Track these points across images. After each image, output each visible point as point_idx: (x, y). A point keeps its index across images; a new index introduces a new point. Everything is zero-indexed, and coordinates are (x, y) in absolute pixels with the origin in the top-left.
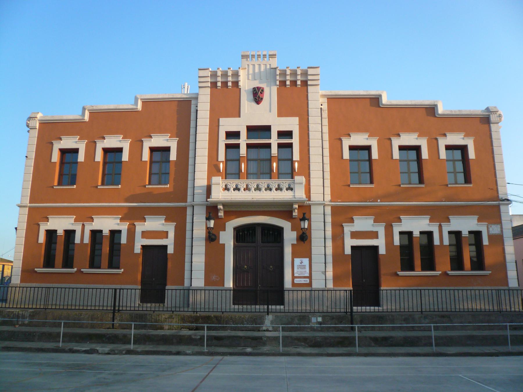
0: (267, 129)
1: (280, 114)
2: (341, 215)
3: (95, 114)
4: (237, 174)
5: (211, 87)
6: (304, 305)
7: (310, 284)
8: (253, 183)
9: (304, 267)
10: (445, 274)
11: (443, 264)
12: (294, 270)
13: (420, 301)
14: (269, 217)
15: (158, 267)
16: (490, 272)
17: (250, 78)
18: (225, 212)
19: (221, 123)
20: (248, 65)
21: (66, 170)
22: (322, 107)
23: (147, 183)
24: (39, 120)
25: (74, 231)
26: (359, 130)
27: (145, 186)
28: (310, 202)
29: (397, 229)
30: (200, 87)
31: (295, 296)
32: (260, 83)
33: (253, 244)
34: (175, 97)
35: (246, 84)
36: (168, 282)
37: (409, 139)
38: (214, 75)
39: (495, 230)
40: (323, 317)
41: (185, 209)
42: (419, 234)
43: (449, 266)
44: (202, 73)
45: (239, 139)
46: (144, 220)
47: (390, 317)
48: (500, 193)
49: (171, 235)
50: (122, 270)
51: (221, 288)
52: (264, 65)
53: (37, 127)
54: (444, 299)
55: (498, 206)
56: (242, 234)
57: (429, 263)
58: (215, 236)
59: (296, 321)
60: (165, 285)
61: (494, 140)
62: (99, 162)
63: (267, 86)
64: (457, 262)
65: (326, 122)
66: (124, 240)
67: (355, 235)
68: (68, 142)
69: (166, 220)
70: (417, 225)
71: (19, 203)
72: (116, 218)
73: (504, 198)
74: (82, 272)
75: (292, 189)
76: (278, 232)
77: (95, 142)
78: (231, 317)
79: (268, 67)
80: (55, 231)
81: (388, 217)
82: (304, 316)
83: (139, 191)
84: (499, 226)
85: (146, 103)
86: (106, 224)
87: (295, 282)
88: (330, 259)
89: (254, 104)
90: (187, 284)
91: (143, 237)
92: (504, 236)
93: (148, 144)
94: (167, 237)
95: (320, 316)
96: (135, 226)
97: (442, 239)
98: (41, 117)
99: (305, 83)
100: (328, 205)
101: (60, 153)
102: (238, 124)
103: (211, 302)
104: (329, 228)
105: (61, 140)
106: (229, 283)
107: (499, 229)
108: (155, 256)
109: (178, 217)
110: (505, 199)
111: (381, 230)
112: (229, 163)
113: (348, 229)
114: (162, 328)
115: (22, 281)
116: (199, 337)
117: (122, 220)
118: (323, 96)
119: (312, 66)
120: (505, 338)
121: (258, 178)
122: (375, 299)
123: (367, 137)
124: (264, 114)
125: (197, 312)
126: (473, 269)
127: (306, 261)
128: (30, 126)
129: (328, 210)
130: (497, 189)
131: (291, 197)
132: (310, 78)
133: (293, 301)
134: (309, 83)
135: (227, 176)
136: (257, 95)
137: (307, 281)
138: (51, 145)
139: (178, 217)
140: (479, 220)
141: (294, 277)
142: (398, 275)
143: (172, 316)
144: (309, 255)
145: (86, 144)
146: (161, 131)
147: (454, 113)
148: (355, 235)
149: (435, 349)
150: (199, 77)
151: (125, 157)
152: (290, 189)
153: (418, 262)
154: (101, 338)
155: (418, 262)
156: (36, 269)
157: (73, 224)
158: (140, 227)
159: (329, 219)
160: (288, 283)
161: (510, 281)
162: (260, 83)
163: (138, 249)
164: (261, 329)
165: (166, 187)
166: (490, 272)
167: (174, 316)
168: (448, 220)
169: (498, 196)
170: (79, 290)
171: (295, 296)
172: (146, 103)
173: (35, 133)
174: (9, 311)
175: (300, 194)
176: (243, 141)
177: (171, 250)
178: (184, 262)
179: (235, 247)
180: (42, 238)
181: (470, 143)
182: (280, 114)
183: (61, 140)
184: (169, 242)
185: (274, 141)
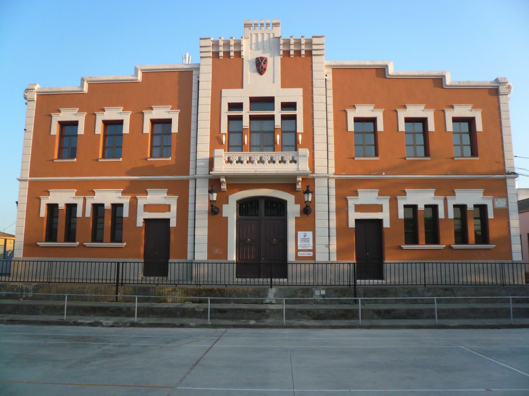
0: (270, 100)
2: (346, 188)
6: (307, 278)
7: (314, 257)
8: (256, 155)
10: (449, 247)
11: (447, 237)
12: (298, 243)
16: (495, 246)
20: (251, 34)
22: (327, 77)
23: (149, 156)
24: (37, 92)
26: (365, 101)
27: (146, 159)
28: (314, 175)
29: (401, 202)
30: (201, 57)
32: (263, 53)
35: (249, 54)
37: (415, 111)
38: (216, 44)
39: (501, 203)
40: (327, 290)
41: (187, 181)
44: (204, 43)
46: (146, 193)
47: (394, 289)
48: (506, 166)
49: (174, 208)
50: (125, 244)
53: (35, 99)
54: (448, 273)
55: (504, 180)
56: (245, 207)
57: (433, 237)
58: (218, 209)
60: (168, 258)
62: (55, 135)
63: (271, 56)
64: (462, 236)
65: (330, 93)
66: (126, 213)
67: (359, 208)
69: (169, 193)
72: (118, 192)
74: (85, 245)
75: (295, 162)
76: (282, 204)
77: (95, 115)
78: (235, 290)
79: (272, 36)
80: (57, 205)
81: (393, 190)
84: (505, 200)
86: (108, 197)
87: (299, 255)
88: (334, 232)
89: (257, 75)
90: (190, 257)
92: (510, 210)
95: (323, 289)
97: (447, 212)
99: (309, 53)
100: (333, 178)
102: (241, 96)
103: (214, 275)
104: (333, 201)
105: (153, 110)
106: (232, 256)
107: (505, 203)
108: (157, 229)
109: (180, 190)
111: (385, 203)
113: (352, 202)
114: (165, 301)
116: (202, 310)
117: (123, 193)
118: (328, 66)
121: (262, 150)
124: (268, 85)
126: (477, 243)
127: (309, 234)
128: (28, 97)
129: (332, 183)
130: (504, 162)
131: (295, 170)
132: (314, 47)
133: (297, 275)
134: (314, 53)
136: (260, 66)
137: (311, 254)
138: (50, 118)
139: (180, 190)
140: (485, 194)
141: (297, 250)
144: (312, 228)
146: (162, 102)
147: (462, 84)
148: (359, 208)
149: (437, 321)
150: (201, 47)
151: (126, 129)
152: (294, 161)
153: (422, 235)
154: (104, 311)
155: (422, 235)
156: (38, 243)
158: (142, 201)
159: (333, 192)
160: (291, 257)
161: (514, 255)
162: (263, 53)
163: (140, 223)
166: (495, 246)
167: (177, 289)
168: (454, 194)
169: (505, 170)
170: (78, 264)
175: (303, 166)
176: (246, 113)
177: (173, 224)
180: (43, 212)
181: (478, 115)
182: (284, 86)
183: (153, 110)
184: (172, 215)
185: (278, 112)
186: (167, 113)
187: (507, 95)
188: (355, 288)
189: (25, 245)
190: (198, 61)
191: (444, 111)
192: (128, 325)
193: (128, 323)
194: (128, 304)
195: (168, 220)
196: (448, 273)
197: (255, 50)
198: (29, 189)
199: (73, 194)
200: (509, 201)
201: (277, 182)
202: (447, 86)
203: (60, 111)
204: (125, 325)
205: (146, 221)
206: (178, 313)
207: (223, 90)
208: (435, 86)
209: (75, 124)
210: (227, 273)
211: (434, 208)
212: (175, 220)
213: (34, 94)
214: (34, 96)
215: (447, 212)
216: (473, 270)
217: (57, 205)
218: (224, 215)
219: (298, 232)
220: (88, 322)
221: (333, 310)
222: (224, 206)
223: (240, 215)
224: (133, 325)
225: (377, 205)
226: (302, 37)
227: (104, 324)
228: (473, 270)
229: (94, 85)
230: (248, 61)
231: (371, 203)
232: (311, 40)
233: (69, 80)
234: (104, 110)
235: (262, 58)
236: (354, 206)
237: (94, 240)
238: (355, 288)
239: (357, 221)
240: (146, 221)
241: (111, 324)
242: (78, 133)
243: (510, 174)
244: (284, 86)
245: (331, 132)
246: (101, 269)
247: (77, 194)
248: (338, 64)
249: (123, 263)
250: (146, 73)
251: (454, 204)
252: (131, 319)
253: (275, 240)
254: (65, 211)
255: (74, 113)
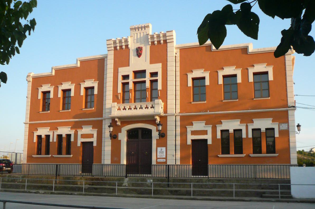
0: (144, 71)
1: (151, 62)
2: (186, 121)
4: (267, 90)
5: (114, 50)
6: (162, 174)
7: (166, 162)
8: (138, 105)
10: (248, 156)
11: (248, 149)
12: (157, 154)
13: (283, 172)
15: (89, 152)
16: (278, 155)
18: (121, 123)
19: (119, 71)
20: (134, 34)
22: (176, 55)
23: (192, 101)
24: (32, 77)
25: (241, 130)
26: (198, 67)
27: (222, 101)
28: (166, 114)
29: (219, 129)
30: (108, 51)
31: (185, 168)
33: (137, 140)
34: (96, 57)
35: (133, 46)
38: (115, 42)
39: (284, 127)
40: (153, 179)
42: (233, 131)
43: (252, 150)
45: (129, 79)
46: (82, 128)
47: (189, 180)
48: (289, 102)
49: (95, 135)
50: (72, 155)
51: (120, 164)
52: (141, 34)
53: (31, 81)
55: (287, 112)
56: (132, 134)
57: (239, 150)
58: (116, 136)
59: (140, 181)
61: (287, 67)
65: (178, 64)
66: (72, 139)
67: (194, 133)
68: (45, 88)
69: (93, 128)
70: (231, 125)
71: (24, 122)
72: (69, 128)
74: (53, 157)
78: (109, 179)
79: (145, 34)
80: (61, 135)
81: (213, 121)
82: (143, 179)
84: (287, 124)
85: (82, 62)
86: (64, 131)
87: (158, 161)
88: (178, 147)
89: (137, 57)
90: (102, 163)
91: (81, 138)
92: (290, 131)
93: (83, 85)
94: (207, 134)
95: (152, 179)
96: (78, 132)
97: (247, 134)
98: (33, 75)
99: (165, 41)
100: (178, 115)
101: (85, 90)
102: (128, 71)
104: (178, 129)
105: (62, 85)
106: (124, 162)
107: (287, 127)
108: (87, 146)
109: (98, 125)
110: (292, 106)
111: (209, 129)
113: (189, 129)
114: (77, 184)
115: (27, 162)
116: (87, 188)
117: (71, 128)
118: (177, 48)
120: (232, 192)
121: (141, 102)
122: (205, 172)
123: (266, 66)
124: (142, 63)
125: (93, 176)
126: (268, 152)
127: (164, 149)
128: (28, 80)
129: (178, 118)
130: (287, 99)
131: (153, 112)
132: (168, 38)
134: (168, 41)
135: (137, 100)
136: (139, 52)
137: (164, 160)
138: (80, 86)
139: (98, 125)
140: (273, 121)
141: (157, 158)
143: (81, 178)
144: (165, 145)
145: (241, 70)
146: (89, 78)
148: (194, 133)
149: (192, 197)
150: (107, 45)
151: (207, 82)
152: (152, 107)
153: (232, 148)
154: (41, 188)
155: (232, 148)
156: (33, 156)
157: (49, 132)
158: (80, 132)
159: (178, 123)
160: (154, 162)
161: (291, 160)
162: (140, 44)
163: (79, 144)
164: (122, 185)
165: (92, 109)
166: (278, 155)
167: (82, 178)
170: (45, 165)
171: (185, 168)
172: (82, 62)
173: (31, 83)
174: (14, 176)
176: (131, 80)
177: (95, 144)
180: (35, 140)
181: (270, 70)
182: (151, 62)
183: (62, 85)
184: (94, 140)
185: (148, 79)
186: (92, 84)
187: (291, 54)
188: (168, 179)
189: (28, 157)
190: (106, 52)
192: (50, 193)
193: (50, 192)
195: (92, 143)
197: (136, 43)
198: (29, 128)
199: (48, 130)
203: (42, 86)
204: (48, 193)
206: (77, 189)
207: (119, 68)
210: (120, 172)
213: (30, 79)
214: (30, 79)
215: (247, 134)
219: (158, 148)
220: (34, 191)
221: (148, 189)
222: (119, 134)
223: (129, 139)
224: (52, 193)
225: (204, 130)
226: (160, 33)
227: (40, 193)
229: (58, 71)
230: (132, 50)
231: (201, 130)
233: (46, 70)
234: (62, 84)
235: (139, 48)
236: (191, 131)
238: (168, 179)
239: (192, 140)
241: (43, 193)
242: (50, 98)
246: (34, 167)
249: (59, 165)
251: (253, 128)
252: (51, 191)
253: (146, 152)
254: (45, 138)
255: (69, 84)
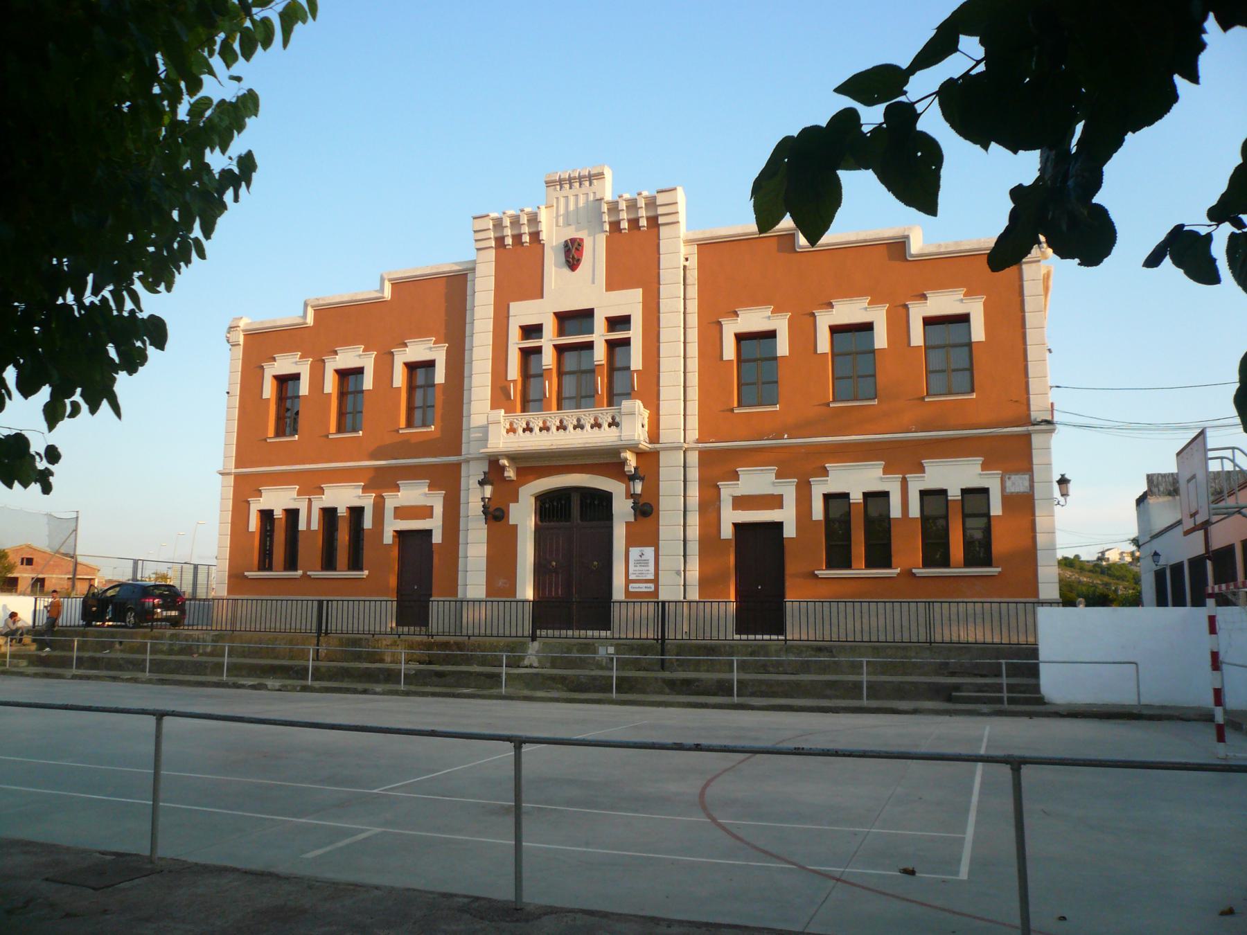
0: (588, 314)
2: (717, 466)
3: (326, 313)
7: (656, 593)
8: (570, 416)
9: (646, 563)
10: (908, 574)
11: (908, 552)
12: (630, 568)
14: (584, 476)
16: (999, 569)
17: (561, 223)
18: (519, 471)
21: (418, 401)
22: (687, 264)
26: (851, 292)
28: (657, 446)
29: (819, 490)
30: (478, 249)
32: (577, 230)
35: (553, 236)
36: (434, 591)
37: (849, 311)
38: (498, 224)
39: (1018, 484)
40: (617, 647)
41: (457, 466)
44: (481, 224)
48: (1032, 408)
49: (438, 511)
50: (366, 572)
52: (579, 198)
53: (241, 342)
54: (905, 623)
55: (1027, 437)
57: (880, 554)
60: (431, 596)
61: (1027, 299)
62: (329, 394)
63: (589, 235)
64: (936, 552)
65: (693, 292)
66: (368, 523)
67: (741, 502)
68: (285, 364)
69: (431, 487)
70: (855, 480)
71: (221, 469)
73: (1039, 420)
75: (617, 425)
76: (606, 498)
77: (323, 361)
79: (591, 198)
80: (335, 510)
81: (802, 467)
83: (389, 439)
84: (1027, 477)
86: (343, 497)
88: (694, 548)
90: (460, 596)
91: (396, 518)
94: (431, 516)
97: (904, 505)
99: (654, 221)
100: (693, 449)
103: (495, 623)
106: (527, 591)
107: (1027, 484)
108: (414, 544)
109: (447, 480)
112: (745, 366)
113: (728, 491)
114: (382, 661)
115: (230, 591)
118: (689, 242)
119: (664, 188)
121: (578, 407)
126: (968, 563)
127: (649, 552)
129: (694, 458)
132: (660, 210)
133: (630, 623)
134: (661, 220)
136: (572, 254)
137: (651, 587)
139: (447, 480)
140: (985, 466)
141: (628, 581)
142: (816, 576)
146: (421, 332)
147: (942, 250)
148: (741, 502)
151: (783, 347)
152: (614, 424)
153: (859, 549)
155: (859, 549)
159: (694, 474)
160: (618, 593)
162: (577, 230)
163: (388, 538)
168: (921, 469)
169: (1029, 415)
172: (398, 285)
175: (635, 429)
176: (548, 341)
177: (437, 538)
178: (458, 557)
179: (538, 531)
180: (254, 524)
182: (610, 286)
184: (435, 524)
185: (600, 336)
188: (663, 644)
189: (230, 577)
190: (471, 255)
191: (906, 307)
194: (216, 659)
195: (428, 533)
196: (905, 623)
200: (1036, 479)
201: (602, 461)
202: (912, 256)
203: (405, 345)
205: (738, 527)
208: (891, 258)
209: (359, 371)
211: (292, 514)
212: (440, 531)
215: (904, 505)
216: (954, 617)
217: (335, 510)
218: (511, 522)
222: (512, 505)
228: (954, 617)
232: (654, 198)
234: (336, 353)
235: (573, 240)
237: (261, 568)
238: (663, 644)
240: (738, 527)
243: (1039, 423)
244: (610, 286)
245: (694, 364)
247: (299, 494)
248: (707, 235)
250: (398, 285)
